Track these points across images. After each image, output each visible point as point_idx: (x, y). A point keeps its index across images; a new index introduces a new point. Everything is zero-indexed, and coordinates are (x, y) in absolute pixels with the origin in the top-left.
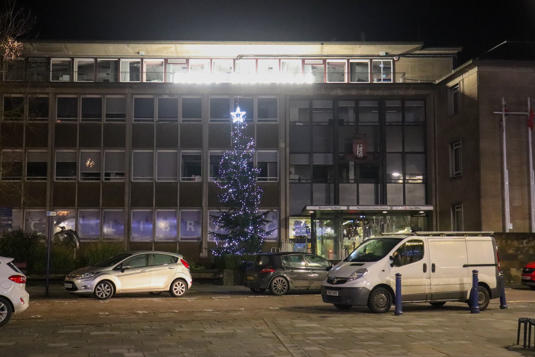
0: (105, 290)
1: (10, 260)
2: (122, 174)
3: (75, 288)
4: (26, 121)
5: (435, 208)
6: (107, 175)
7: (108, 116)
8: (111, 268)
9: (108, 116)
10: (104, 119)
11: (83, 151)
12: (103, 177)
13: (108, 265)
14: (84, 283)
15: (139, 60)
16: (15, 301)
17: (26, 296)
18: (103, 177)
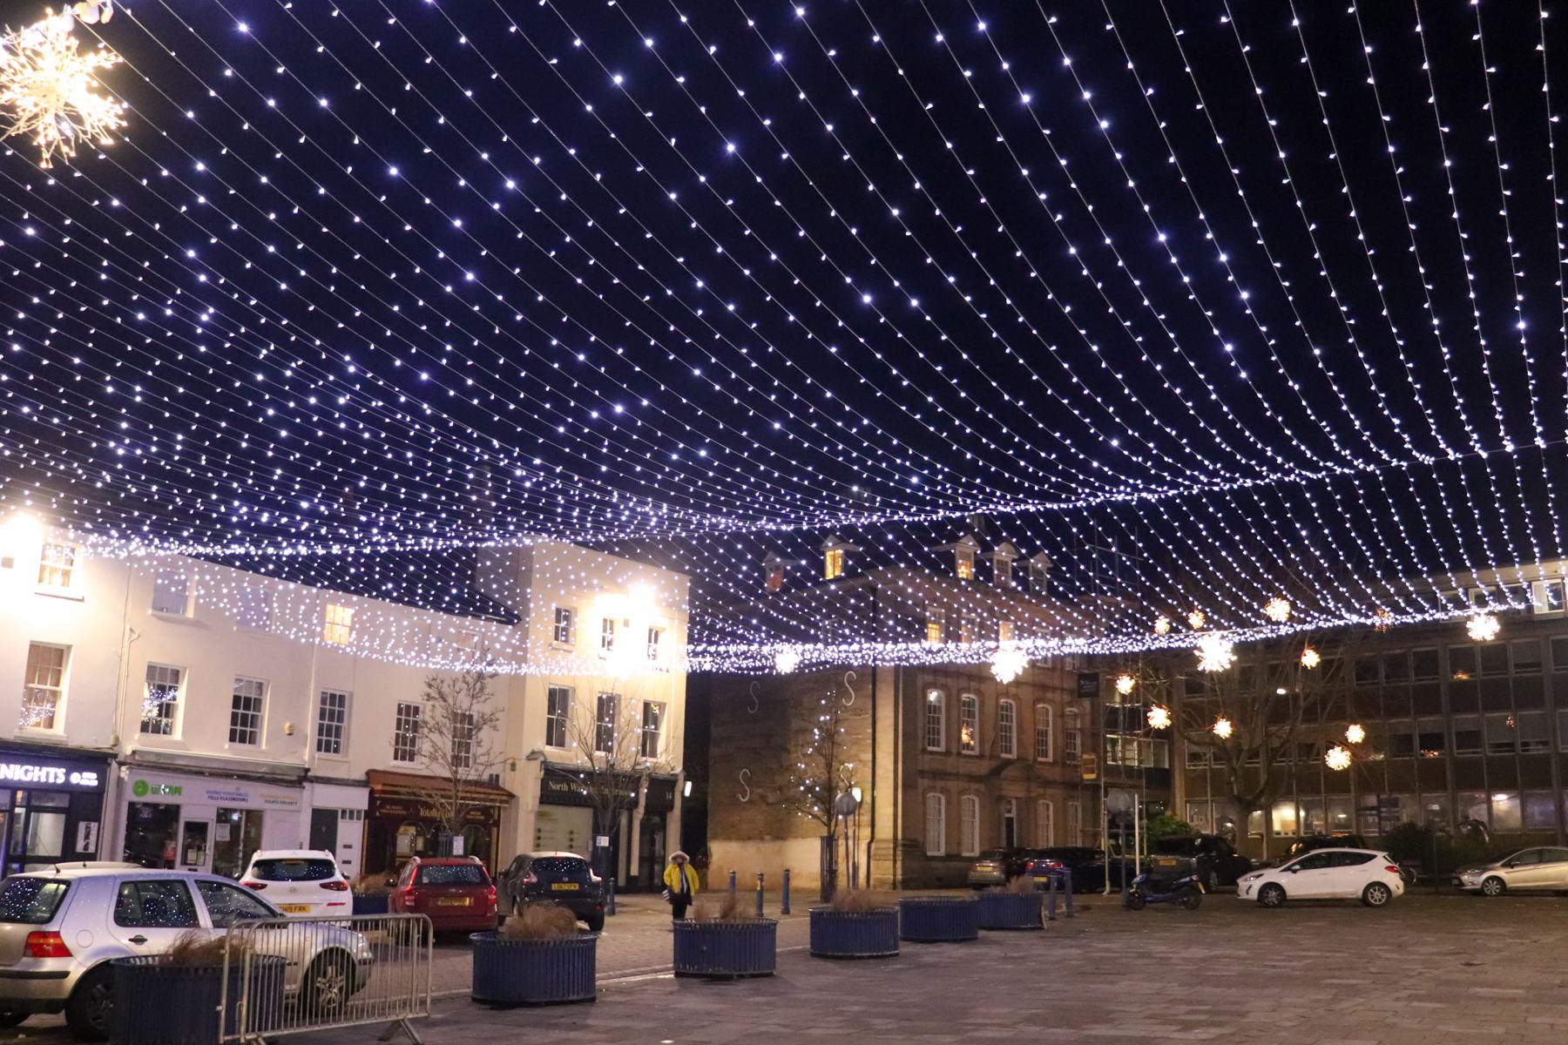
0: (1494, 888)
1: (1385, 854)
2: (1545, 743)
3: (1462, 884)
4: (1413, 680)
5: (645, 871)
6: (1525, 744)
7: (1517, 666)
8: (1498, 864)
9: (1517, 666)
10: (1512, 671)
11: (1488, 715)
12: (1519, 748)
13: (1497, 861)
14: (1471, 879)
15: (1559, 581)
16: (1392, 887)
17: (1401, 884)
18: (1519, 748)
